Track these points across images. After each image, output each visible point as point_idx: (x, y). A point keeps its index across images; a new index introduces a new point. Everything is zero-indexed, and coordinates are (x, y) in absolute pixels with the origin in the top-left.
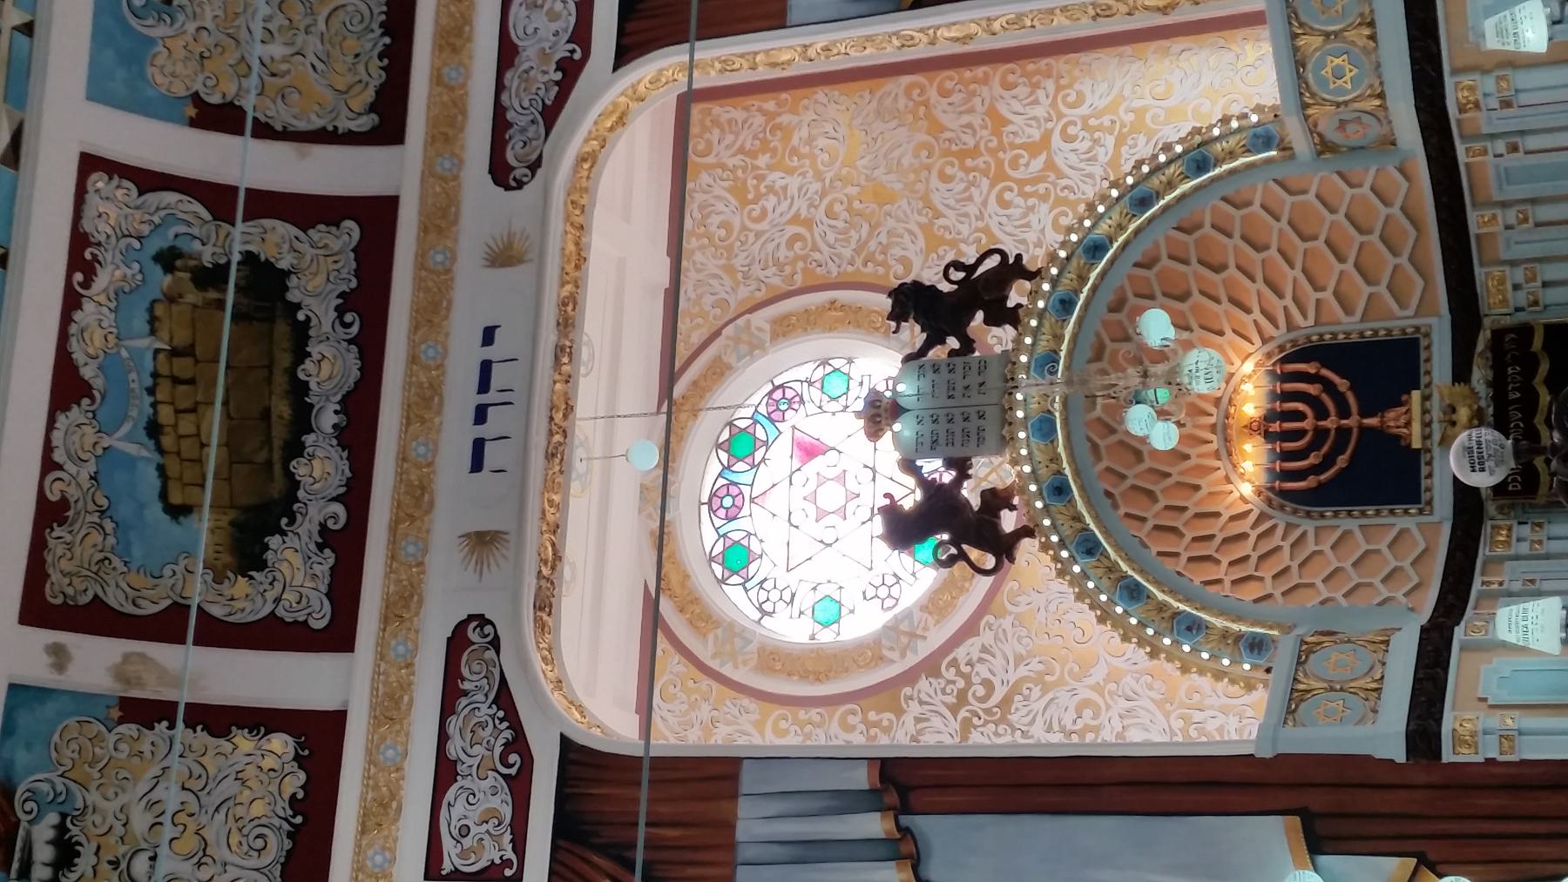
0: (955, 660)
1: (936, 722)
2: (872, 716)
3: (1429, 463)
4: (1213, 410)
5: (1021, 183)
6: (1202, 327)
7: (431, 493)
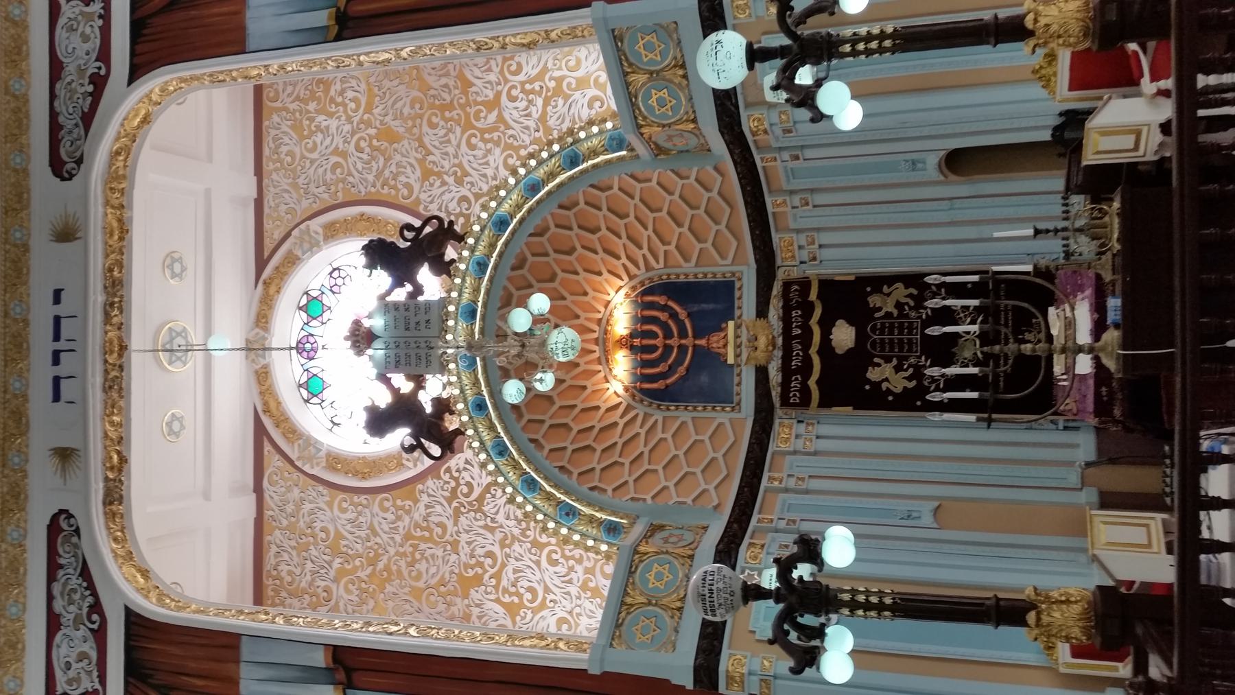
0: (449, 467)
1: (438, 508)
2: (399, 502)
3: (739, 375)
4: (596, 328)
5: (483, 131)
6: (586, 270)
7: (27, 417)
